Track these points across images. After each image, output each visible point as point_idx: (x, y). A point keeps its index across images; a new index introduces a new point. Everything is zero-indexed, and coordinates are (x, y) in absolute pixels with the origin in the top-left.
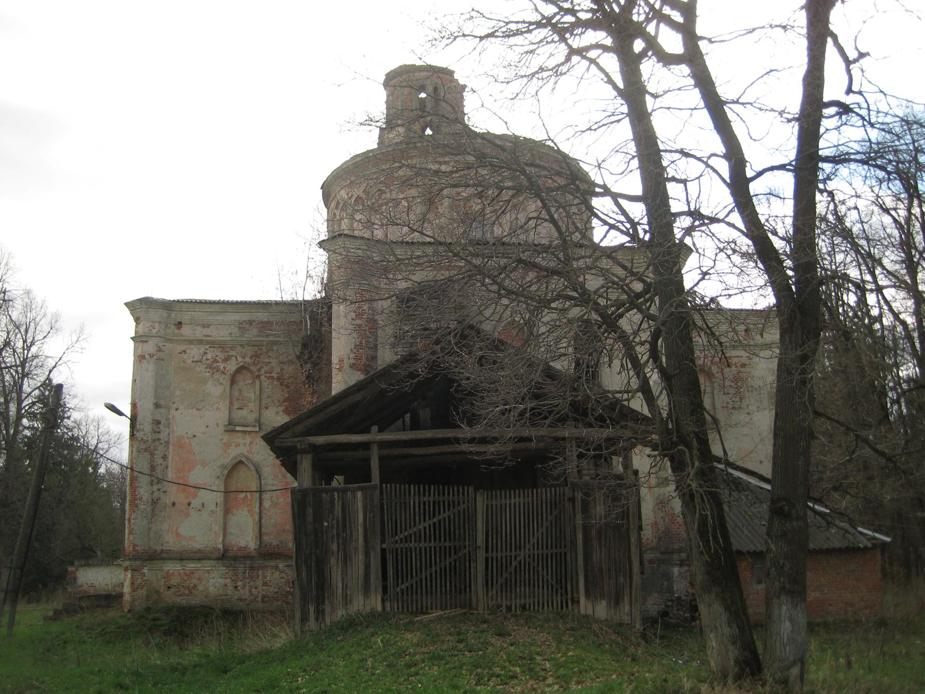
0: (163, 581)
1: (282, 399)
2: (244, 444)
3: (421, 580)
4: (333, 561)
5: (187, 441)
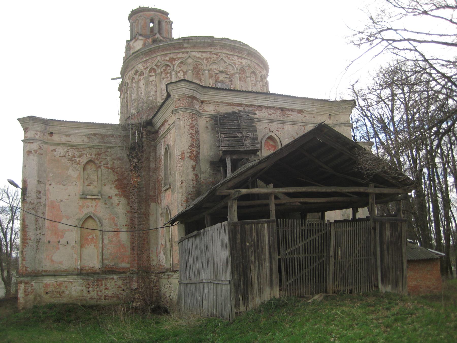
0: (43, 289)
1: (114, 180)
2: (92, 206)
3: (300, 276)
4: (252, 267)
5: (57, 204)
